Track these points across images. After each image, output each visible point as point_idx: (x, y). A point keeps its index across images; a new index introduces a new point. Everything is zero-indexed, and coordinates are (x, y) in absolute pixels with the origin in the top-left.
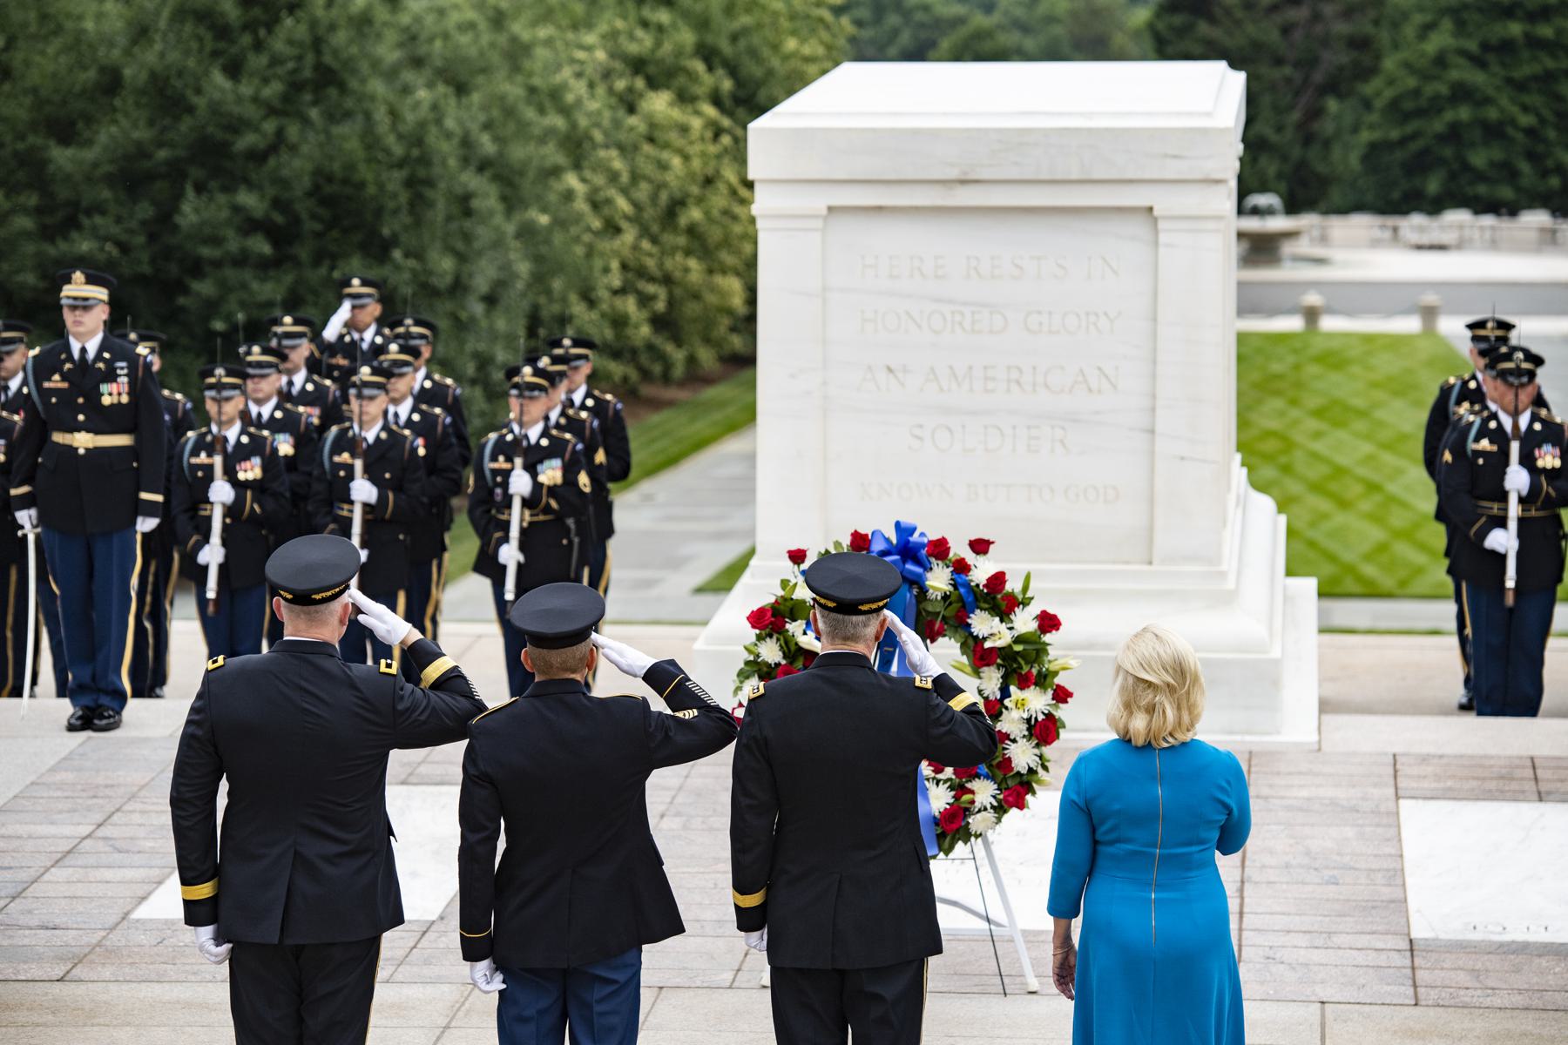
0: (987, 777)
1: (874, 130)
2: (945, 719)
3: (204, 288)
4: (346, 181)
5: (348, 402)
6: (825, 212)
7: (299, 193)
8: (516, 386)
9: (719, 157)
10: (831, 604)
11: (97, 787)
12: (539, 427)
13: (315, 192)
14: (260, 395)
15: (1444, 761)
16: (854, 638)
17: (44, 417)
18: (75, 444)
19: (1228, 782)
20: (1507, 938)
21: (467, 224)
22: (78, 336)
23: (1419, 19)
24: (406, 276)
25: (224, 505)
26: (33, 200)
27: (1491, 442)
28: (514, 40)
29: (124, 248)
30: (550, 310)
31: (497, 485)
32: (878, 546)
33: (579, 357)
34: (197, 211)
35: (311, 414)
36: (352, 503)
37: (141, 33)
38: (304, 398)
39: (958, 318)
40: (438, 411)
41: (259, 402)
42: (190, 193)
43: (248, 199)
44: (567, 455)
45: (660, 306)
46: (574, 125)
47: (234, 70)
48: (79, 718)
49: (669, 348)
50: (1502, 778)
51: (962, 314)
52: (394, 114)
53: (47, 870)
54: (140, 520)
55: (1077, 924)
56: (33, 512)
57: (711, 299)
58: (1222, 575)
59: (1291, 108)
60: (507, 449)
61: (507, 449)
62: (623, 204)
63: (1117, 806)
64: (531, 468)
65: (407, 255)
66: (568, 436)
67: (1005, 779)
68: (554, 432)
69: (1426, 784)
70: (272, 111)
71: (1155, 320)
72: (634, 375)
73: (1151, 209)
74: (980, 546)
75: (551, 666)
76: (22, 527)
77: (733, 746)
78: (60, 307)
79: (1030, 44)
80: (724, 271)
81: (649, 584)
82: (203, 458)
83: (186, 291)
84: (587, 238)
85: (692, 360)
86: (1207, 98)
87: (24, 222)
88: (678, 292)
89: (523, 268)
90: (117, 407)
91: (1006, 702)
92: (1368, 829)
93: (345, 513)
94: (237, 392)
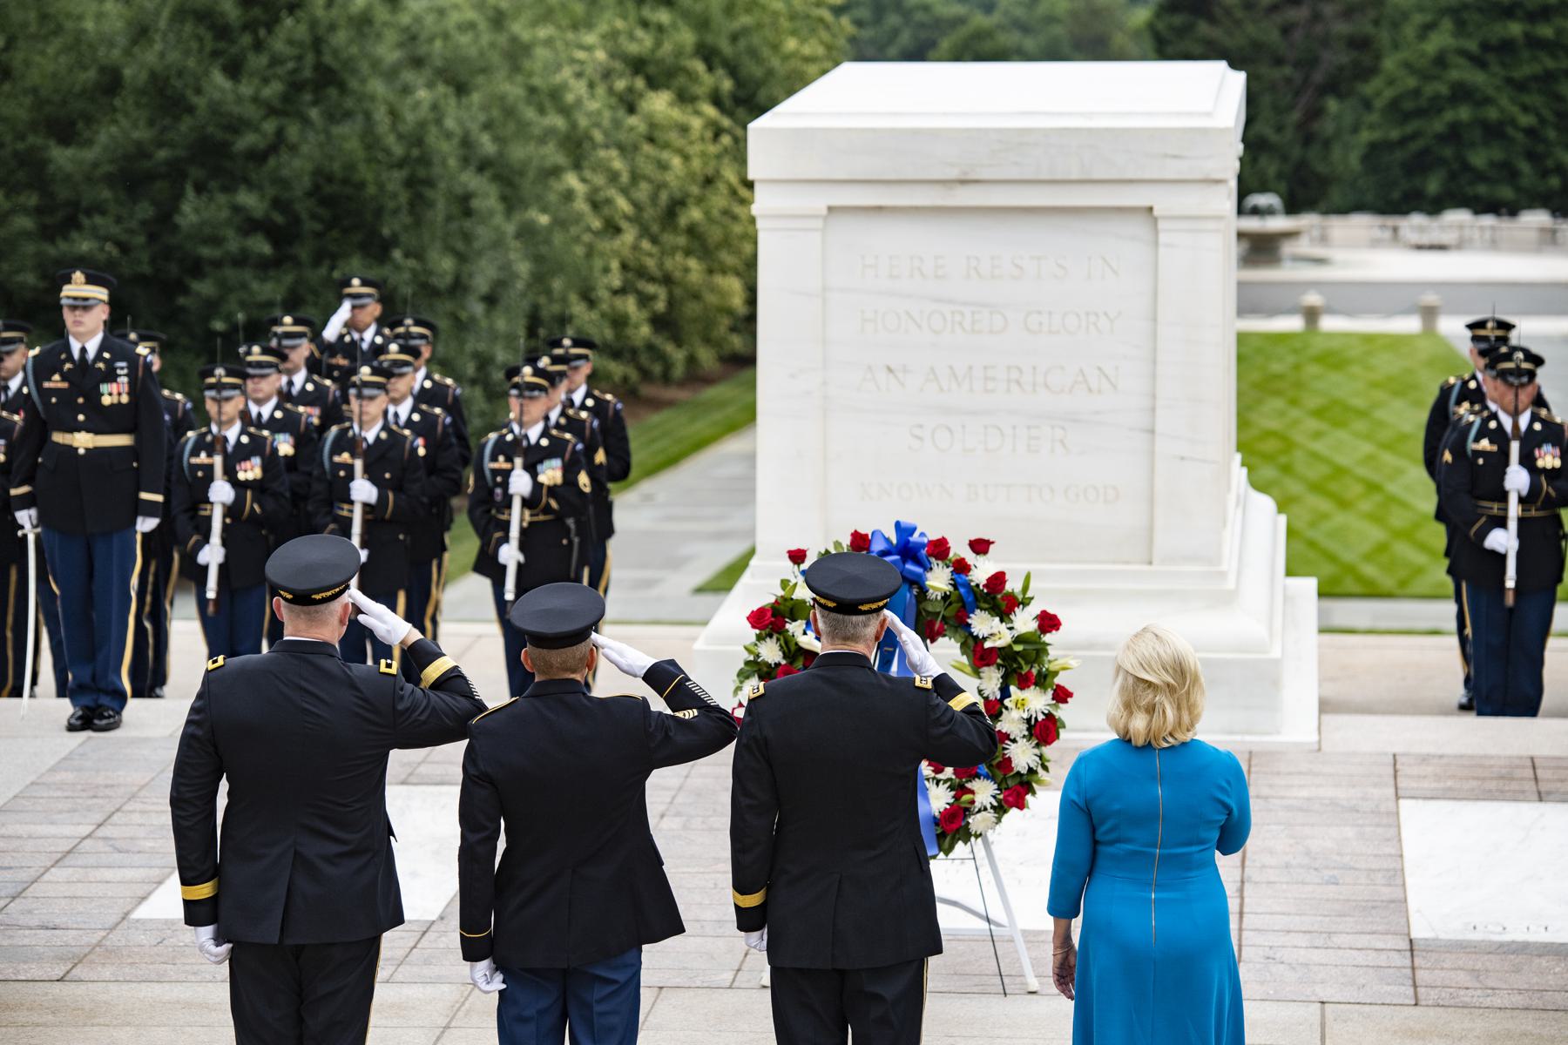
0: (987, 777)
1: (874, 130)
2: (945, 719)
3: (204, 288)
4: (346, 181)
5: (348, 402)
6: (825, 212)
7: (299, 193)
8: (516, 386)
9: (719, 157)
10: (831, 604)
11: (97, 787)
12: (539, 427)
13: (315, 192)
14: (260, 395)
15: (1444, 761)
16: (854, 638)
17: (44, 417)
18: (75, 444)
19: (1228, 782)
20: (1507, 938)
21: (467, 224)
22: (78, 336)
23: (1419, 19)
24: (406, 276)
25: (224, 505)
26: (33, 200)
27: (1491, 442)
28: (514, 40)
29: (124, 248)
30: (550, 310)
31: (497, 485)
32: (878, 546)
33: (579, 357)
34: (197, 211)
35: (311, 414)
36: (352, 503)
37: (141, 33)
38: (304, 398)
39: (958, 318)
40: (438, 411)
41: (259, 402)
42: (190, 193)
43: (248, 199)
44: (567, 455)
45: (660, 306)
46: (574, 125)
47: (234, 70)
48: (79, 718)
49: (669, 348)
50: (1502, 778)
51: (962, 314)
52: (394, 114)
53: (47, 870)
54: (140, 520)
55: (1077, 924)
56: (33, 512)
57: (711, 299)
58: (1222, 575)
59: (1291, 108)
60: (507, 449)
61: (507, 449)
62: (623, 204)
63: (1117, 806)
64: (531, 468)
65: (407, 255)
66: (568, 436)
67: (1005, 779)
68: (554, 432)
69: (1426, 784)
70: (272, 111)
71: (1155, 320)
72: (634, 375)
73: (1151, 209)
74: (980, 546)
75: (551, 666)
76: (22, 527)
77: (733, 746)
78: (60, 307)
79: (1030, 44)
80: (724, 271)
81: (649, 584)
82: (203, 458)
83: (186, 291)
84: (587, 238)
85: (692, 360)
86: (1207, 98)
87: (24, 222)
88: (678, 292)
89: (523, 268)
90: (117, 407)
91: (1006, 702)
92: (1368, 829)
93: (345, 513)
94: (237, 392)
